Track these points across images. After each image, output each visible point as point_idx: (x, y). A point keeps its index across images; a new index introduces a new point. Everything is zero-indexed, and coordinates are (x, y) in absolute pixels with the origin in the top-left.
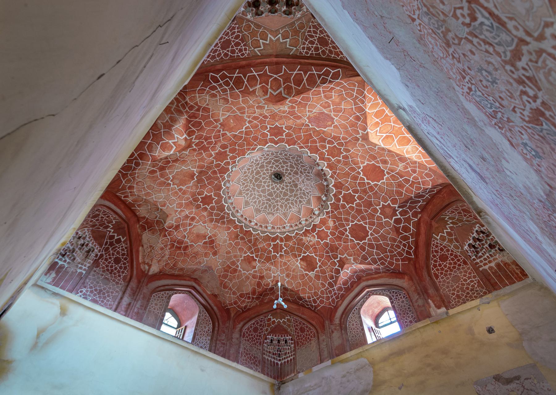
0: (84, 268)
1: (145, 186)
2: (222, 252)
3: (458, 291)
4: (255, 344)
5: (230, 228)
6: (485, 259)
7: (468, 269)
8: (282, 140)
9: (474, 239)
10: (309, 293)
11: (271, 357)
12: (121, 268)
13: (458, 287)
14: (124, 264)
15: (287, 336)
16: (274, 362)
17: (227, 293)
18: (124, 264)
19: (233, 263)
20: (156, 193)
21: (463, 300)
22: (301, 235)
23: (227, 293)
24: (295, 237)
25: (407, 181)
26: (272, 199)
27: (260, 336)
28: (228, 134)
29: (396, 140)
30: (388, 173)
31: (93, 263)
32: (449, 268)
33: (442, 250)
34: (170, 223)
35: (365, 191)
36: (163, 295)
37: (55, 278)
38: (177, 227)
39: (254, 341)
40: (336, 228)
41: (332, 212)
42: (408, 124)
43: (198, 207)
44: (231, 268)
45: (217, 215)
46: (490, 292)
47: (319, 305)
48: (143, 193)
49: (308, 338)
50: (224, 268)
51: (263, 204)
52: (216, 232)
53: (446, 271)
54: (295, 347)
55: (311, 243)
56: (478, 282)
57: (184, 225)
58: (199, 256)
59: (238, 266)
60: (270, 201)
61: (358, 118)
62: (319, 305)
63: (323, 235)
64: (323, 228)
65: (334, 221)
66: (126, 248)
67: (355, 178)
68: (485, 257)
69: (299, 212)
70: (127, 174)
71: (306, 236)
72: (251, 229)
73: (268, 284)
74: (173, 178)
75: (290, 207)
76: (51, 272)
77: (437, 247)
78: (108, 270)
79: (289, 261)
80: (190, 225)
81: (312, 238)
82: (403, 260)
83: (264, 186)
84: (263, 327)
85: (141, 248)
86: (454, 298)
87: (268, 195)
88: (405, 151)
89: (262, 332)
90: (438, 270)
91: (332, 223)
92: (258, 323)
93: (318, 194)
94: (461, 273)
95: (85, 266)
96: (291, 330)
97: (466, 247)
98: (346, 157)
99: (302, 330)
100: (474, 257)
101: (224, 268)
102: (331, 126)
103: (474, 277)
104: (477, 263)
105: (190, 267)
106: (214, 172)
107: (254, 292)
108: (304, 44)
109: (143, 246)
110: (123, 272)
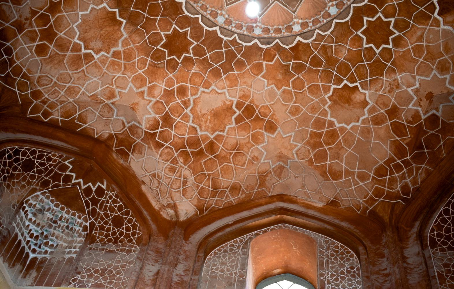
0: (73, 250)
1: (55, 80)
2: (281, 113)
12: (128, 229)
14: (130, 221)
17: (347, 184)
18: (130, 221)
19: (319, 123)
20: (81, 82)
23: (347, 184)
31: (85, 240)
34: (148, 120)
36: (232, 245)
37: (36, 277)
38: (167, 120)
43: (172, 66)
44: (321, 134)
48: (62, 93)
50: (308, 143)
57: (176, 110)
58: (246, 149)
59: (331, 124)
66: (117, 196)
70: (8, 75)
72: (299, 38)
73: (416, 116)
74: (84, 41)
76: (31, 272)
78: (110, 240)
79: (420, 38)
80: (186, 104)
85: (143, 188)
95: (75, 248)
101: (308, 143)
105: (241, 176)
107: (399, 150)
109: (143, 183)
110: (134, 234)
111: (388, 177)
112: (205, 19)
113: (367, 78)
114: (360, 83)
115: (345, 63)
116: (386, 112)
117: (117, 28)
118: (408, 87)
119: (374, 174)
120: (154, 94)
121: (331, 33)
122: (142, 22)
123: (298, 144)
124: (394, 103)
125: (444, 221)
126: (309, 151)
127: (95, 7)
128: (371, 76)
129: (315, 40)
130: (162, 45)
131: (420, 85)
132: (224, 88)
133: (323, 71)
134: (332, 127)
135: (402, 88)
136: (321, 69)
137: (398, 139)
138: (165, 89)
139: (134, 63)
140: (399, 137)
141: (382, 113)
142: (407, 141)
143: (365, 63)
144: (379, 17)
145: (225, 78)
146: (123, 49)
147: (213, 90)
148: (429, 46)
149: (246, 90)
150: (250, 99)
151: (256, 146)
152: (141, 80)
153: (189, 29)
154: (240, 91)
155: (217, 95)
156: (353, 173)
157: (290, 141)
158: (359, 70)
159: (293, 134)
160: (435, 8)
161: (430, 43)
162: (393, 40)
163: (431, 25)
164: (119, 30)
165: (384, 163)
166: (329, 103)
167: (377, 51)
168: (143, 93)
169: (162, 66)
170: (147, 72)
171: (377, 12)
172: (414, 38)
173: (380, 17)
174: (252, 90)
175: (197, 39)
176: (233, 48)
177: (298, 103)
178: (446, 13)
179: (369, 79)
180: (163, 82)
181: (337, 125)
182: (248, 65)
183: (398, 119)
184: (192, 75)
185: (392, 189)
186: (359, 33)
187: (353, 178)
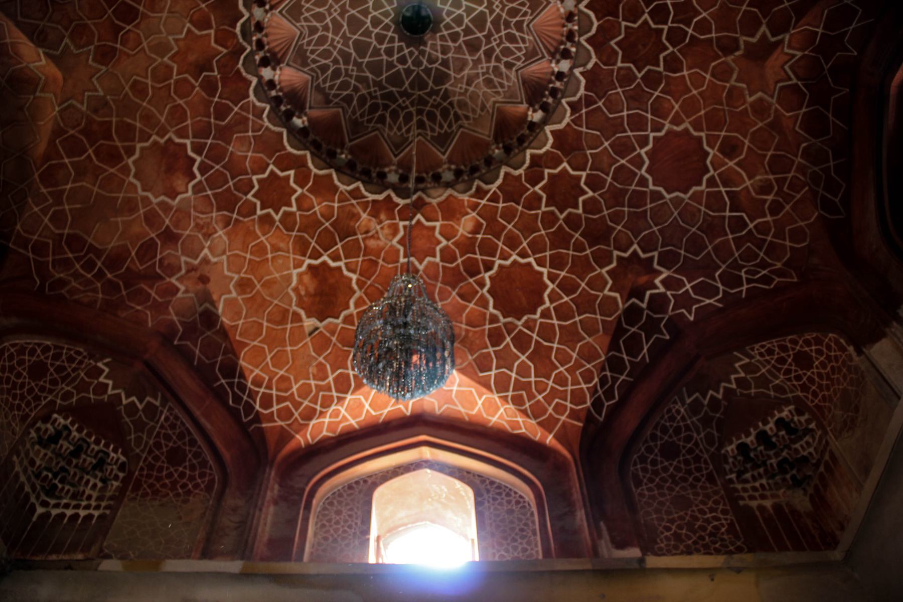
3: (680, 527)
4: (12, 408)
5: (204, 24)
6: (755, 489)
7: (716, 493)
9: (763, 437)
10: (265, 369)
11: (29, 479)
13: (681, 518)
15: (115, 451)
16: (27, 496)
19: (127, 132)
21: (688, 547)
25: (738, 224)
26: (356, 63)
27: (37, 398)
29: (804, 110)
30: (711, 182)
32: (672, 476)
33: (677, 431)
39: (15, 397)
40: (467, 246)
41: (494, 199)
44: (110, 138)
46: (751, 550)
47: (270, 418)
49: (184, 486)
51: (326, 54)
53: (664, 480)
54: (122, 491)
55: (372, 243)
56: (731, 525)
59: (130, 151)
60: (347, 62)
62: (270, 418)
63: (421, 243)
64: (437, 224)
67: (623, 148)
68: (757, 484)
71: (375, 214)
77: (672, 419)
81: (387, 231)
82: (574, 415)
84: (64, 379)
86: (666, 537)
87: (356, 43)
89: (51, 391)
90: (645, 470)
91: (470, 226)
92: (57, 357)
94: (696, 494)
96: (139, 440)
97: (731, 448)
99: (176, 456)
100: (733, 476)
103: (724, 512)
104: (736, 490)
111: (71, 255)
113: (211, 189)
114: (200, 182)
116: (168, 227)
118: (210, 248)
119: (68, 235)
121: (267, 128)
123: (85, 105)
124: (182, 235)
125: (32, 352)
126: (79, 125)
128: (214, 195)
129: (254, 106)
131: (216, 263)
133: (210, 123)
134: (126, 153)
135: (206, 241)
136: (212, 120)
137: (133, 254)
140: (137, 254)
141: (164, 222)
142: (133, 267)
143: (231, 183)
150: (149, 13)
151: (67, 34)
156: (60, 203)
157: (89, 91)
159: (101, 93)
162: (268, 215)
163: (294, 259)
165: (91, 245)
166: (162, 141)
167: (249, 196)
171: (302, 187)
172: (274, 241)
174: (165, 15)
177: (153, 92)
181: (130, 161)
182: (207, 6)
183: (162, 246)
185: (54, 267)
186: (271, 167)
187: (51, 206)
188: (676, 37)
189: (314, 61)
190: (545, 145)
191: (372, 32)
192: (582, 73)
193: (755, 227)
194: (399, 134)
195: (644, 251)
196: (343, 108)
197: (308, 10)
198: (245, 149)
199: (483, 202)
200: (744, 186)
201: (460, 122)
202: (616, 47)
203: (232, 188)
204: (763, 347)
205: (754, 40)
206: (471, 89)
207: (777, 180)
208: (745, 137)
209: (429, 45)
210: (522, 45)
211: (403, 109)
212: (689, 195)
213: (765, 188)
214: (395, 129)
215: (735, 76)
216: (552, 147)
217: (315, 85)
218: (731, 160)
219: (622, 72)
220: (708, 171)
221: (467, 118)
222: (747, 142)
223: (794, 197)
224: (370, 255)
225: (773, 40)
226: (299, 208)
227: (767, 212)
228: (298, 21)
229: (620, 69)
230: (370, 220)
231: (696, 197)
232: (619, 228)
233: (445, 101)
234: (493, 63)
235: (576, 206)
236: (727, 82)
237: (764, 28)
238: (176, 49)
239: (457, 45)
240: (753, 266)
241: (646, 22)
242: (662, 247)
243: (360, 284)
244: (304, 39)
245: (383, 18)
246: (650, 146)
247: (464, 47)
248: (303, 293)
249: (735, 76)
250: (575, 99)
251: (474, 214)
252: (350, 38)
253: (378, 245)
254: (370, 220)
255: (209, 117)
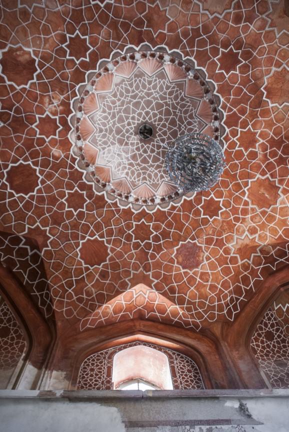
8: (198, 200)
22: (68, 98)
24: (73, 87)
25: (70, 285)
28: (258, 176)
30: (87, 269)
35: (75, 226)
40: (46, 153)
41: (71, 167)
42: (220, 399)
45: (202, 43)
52: (188, 10)
55: (47, 100)
60: (132, 97)
61: (172, 290)
63: (47, 127)
65: (57, 159)
69: (92, 118)
75: (104, 111)
81: (54, 109)
83: (152, 109)
88: (110, 306)
90: (258, 346)
91: (56, 154)
93: (100, 162)
98: (129, 238)
102: (176, 256)
106: (243, 111)
108: (275, 319)
112: (204, 77)
115: (103, 23)
117: (270, 85)
120: (262, 22)
122: (249, 85)
127: (278, 106)
130: (240, 63)
132: (203, 14)
138: (251, 24)
139: (268, 54)
144: (78, 60)
145: (199, 24)
146: (271, 68)
147: (212, 14)
148: (38, 34)
149: (185, 9)
152: (268, 36)
153: (217, 72)
154: (190, 9)
155: (210, 9)
158: (180, 278)
160: (38, 65)
161: (38, 37)
164: (268, 84)
168: (271, 26)
169: (246, 46)
170: (261, 43)
171: (79, 64)
172: (50, 41)
173: (78, 60)
175: (214, 63)
176: (188, 50)
178: (30, 61)
179: (83, 7)
180: (251, 31)
184: (225, 32)
188: (148, 246)
189: (136, 81)
190: (97, 191)
191: (143, 111)
192: (130, 207)
193: (70, 293)
194: (97, 119)
195: (50, 243)
196: (112, 92)
197: (160, 82)
198: (103, 35)
199: (69, 161)
200: (88, 284)
201: (102, 150)
202: (141, 221)
203: (83, 22)
204: (8, 310)
205: (151, 278)
206: (116, 156)
207: (93, 298)
208: (110, 281)
209: (135, 137)
210: (136, 180)
211: (108, 122)
212: (79, 259)
213: (89, 294)
214: (99, 118)
215: (135, 272)
216: (96, 195)
217: (125, 79)
218: (99, 276)
219: (131, 225)
220: (92, 267)
221: (104, 153)
222: (108, 282)
223: (87, 307)
224: (40, 98)
225: (152, 285)
226: (68, 60)
227: (78, 296)
228: (156, 77)
229: (132, 224)
230: (59, 100)
231: (80, 263)
232: (61, 229)
233: (111, 143)
234: (128, 166)
235: (69, 207)
236: (132, 270)
237: (156, 281)
238: (161, 9)
239: (135, 150)
240: (51, 295)
241: (153, 233)
242: (54, 251)
243: (24, 90)
244: (147, 78)
245: (149, 117)
246: (99, 239)
247: (134, 153)
248: (18, 53)
249: (135, 272)
250: (118, 205)
251: (63, 156)
252: (142, 100)
253: (45, 103)
254: (59, 100)
255: (123, 19)
